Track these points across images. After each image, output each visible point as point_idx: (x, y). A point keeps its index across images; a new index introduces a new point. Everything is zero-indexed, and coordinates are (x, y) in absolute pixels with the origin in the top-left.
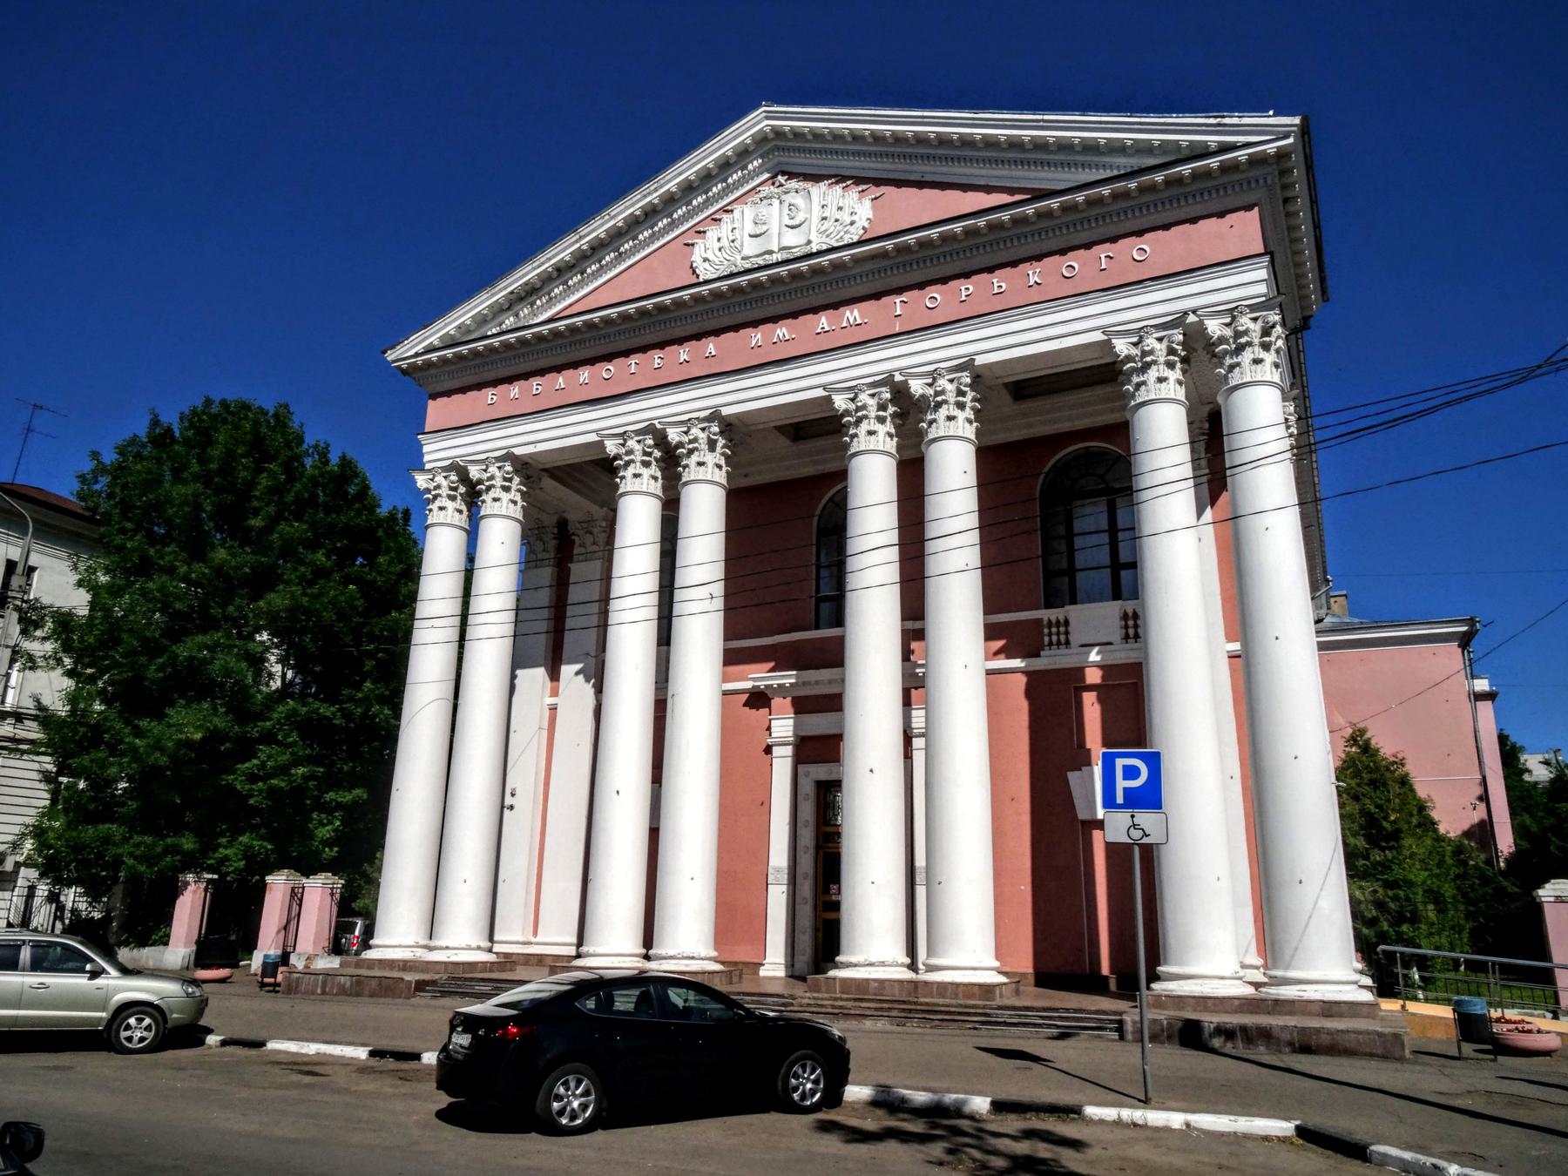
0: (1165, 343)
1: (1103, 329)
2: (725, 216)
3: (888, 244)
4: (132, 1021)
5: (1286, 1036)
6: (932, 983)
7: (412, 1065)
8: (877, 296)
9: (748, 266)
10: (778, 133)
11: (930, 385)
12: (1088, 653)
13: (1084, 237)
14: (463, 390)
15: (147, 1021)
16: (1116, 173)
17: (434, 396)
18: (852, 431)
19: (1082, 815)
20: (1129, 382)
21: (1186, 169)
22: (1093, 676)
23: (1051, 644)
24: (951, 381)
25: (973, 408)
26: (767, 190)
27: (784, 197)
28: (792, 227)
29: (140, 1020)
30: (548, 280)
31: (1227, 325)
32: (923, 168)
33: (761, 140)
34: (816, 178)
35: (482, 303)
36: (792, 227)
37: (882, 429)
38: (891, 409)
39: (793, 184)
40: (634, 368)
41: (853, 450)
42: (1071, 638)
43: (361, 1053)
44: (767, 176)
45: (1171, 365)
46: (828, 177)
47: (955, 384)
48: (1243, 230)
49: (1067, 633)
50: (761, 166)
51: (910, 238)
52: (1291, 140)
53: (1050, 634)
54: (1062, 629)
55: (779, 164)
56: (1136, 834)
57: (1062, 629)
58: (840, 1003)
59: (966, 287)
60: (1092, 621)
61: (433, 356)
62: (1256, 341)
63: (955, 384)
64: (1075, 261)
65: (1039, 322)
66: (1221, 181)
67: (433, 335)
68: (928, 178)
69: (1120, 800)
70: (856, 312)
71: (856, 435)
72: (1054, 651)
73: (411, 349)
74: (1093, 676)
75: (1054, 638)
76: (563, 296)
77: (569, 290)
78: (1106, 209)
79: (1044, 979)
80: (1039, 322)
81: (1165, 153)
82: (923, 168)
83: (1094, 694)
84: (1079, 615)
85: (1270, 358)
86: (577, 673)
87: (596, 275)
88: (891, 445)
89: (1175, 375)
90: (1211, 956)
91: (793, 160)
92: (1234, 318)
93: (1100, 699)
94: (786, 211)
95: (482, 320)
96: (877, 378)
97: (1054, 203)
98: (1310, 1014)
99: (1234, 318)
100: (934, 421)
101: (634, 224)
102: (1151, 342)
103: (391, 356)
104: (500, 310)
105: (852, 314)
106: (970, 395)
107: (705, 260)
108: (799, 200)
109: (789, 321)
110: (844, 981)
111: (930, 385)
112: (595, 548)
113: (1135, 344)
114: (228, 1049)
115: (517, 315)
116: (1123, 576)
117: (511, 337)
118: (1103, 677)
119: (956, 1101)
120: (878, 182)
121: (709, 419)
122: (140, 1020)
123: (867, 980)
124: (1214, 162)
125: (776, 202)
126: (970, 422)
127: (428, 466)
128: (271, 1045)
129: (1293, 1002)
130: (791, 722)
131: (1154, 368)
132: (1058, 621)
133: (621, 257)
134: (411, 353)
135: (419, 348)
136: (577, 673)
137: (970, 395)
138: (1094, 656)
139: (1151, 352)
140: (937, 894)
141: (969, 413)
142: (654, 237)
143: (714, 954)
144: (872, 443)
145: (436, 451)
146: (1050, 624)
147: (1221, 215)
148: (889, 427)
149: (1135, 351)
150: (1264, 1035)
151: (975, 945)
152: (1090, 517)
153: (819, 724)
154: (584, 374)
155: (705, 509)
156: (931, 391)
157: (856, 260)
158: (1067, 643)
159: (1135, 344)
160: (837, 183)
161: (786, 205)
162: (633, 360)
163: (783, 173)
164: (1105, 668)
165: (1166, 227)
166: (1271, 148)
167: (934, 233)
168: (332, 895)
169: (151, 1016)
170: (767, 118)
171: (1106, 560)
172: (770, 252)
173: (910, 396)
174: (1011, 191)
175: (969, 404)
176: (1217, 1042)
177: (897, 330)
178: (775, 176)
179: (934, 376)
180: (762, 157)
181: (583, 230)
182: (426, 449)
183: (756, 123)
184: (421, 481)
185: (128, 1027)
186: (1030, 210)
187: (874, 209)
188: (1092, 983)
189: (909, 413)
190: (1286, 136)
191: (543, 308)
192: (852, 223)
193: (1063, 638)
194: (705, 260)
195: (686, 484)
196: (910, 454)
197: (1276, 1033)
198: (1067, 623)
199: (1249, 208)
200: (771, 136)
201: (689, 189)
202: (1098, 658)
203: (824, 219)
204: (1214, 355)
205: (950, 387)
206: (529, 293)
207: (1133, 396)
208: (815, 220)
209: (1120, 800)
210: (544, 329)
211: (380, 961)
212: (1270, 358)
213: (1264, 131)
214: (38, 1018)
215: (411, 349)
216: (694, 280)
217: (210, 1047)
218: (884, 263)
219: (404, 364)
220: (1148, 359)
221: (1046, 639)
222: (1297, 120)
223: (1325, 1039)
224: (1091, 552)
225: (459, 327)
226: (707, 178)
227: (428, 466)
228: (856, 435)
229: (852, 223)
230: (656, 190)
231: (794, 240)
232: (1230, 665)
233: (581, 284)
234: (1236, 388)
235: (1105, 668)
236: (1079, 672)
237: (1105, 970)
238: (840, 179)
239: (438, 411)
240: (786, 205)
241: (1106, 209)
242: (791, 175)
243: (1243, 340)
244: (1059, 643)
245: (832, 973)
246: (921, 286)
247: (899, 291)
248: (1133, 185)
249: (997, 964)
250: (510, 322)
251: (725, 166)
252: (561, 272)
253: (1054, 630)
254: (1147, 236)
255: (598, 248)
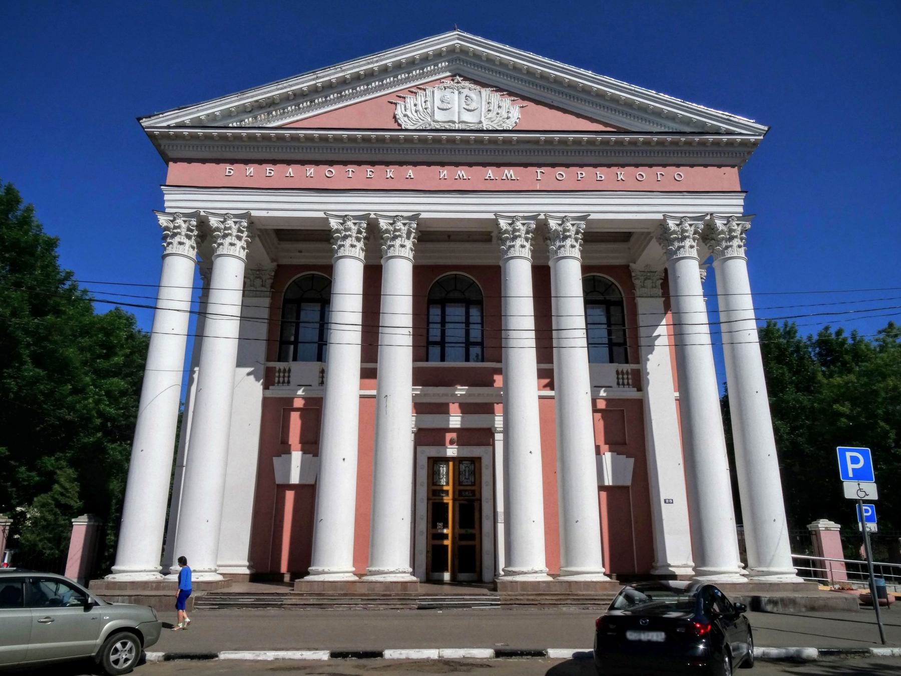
0: (237, 226)
1: (325, 211)
2: (421, 92)
3: (543, 136)
4: (118, 645)
5: (803, 602)
6: (580, 582)
7: (376, 662)
8: (526, 165)
9: (438, 127)
10: (464, 51)
11: (222, 222)
12: (297, 390)
13: (622, 160)
14: (204, 161)
15: (118, 645)
16: (667, 130)
17: (176, 161)
18: (219, 241)
19: (279, 480)
20: (504, 244)
21: (711, 138)
22: (299, 403)
23: (279, 382)
24: (355, 224)
25: (246, 241)
26: (448, 82)
27: (461, 90)
28: (468, 110)
29: (124, 644)
30: (287, 99)
31: (725, 225)
32: (554, 97)
33: (452, 50)
34: (484, 85)
35: (232, 102)
36: (468, 110)
37: (188, 243)
38: (196, 233)
39: (467, 84)
40: (336, 174)
41: (218, 253)
42: (291, 379)
43: (485, 653)
44: (448, 74)
45: (358, 239)
46: (492, 86)
47: (187, 224)
48: (730, 177)
49: (289, 377)
50: (446, 67)
51: (557, 136)
52: (762, 137)
53: (279, 377)
54: (287, 374)
55: (458, 69)
56: (862, 494)
57: (287, 374)
58: (530, 597)
59: (601, 172)
60: (302, 370)
61: (186, 131)
62: (523, 235)
63: (187, 224)
64: (643, 172)
65: (625, 201)
66: (501, 147)
67: (187, 115)
68: (555, 104)
69: (851, 475)
70: (511, 172)
71: (222, 244)
72: (281, 387)
73: (164, 121)
74: (299, 403)
75: (281, 380)
76: (293, 114)
77: (299, 110)
78: (414, 146)
79: (255, 578)
80: (625, 201)
81: (696, 127)
82: (554, 97)
83: (299, 413)
84: (297, 368)
85: (239, 244)
86: (249, 374)
87: (320, 105)
88: (193, 254)
89: (360, 245)
90: (335, 560)
91: (468, 69)
92: (728, 222)
93: (301, 417)
94: (463, 99)
95: (228, 114)
96: (526, 214)
97: (627, 138)
98: (787, 591)
99: (728, 222)
100: (171, 243)
101: (357, 79)
102: (519, 225)
103: (145, 122)
104: (244, 111)
105: (509, 172)
106: (245, 234)
107: (405, 115)
108: (473, 95)
109: (467, 168)
110: (524, 583)
111: (222, 222)
112: (263, 289)
113: (510, 224)
114: (172, 663)
115: (256, 118)
116: (320, 350)
117: (244, 132)
118: (305, 405)
119: (797, 651)
120: (524, 98)
121: (411, 218)
122: (124, 644)
123: (539, 582)
124: (725, 138)
125: (456, 92)
126: (244, 248)
127: (167, 210)
128: (223, 656)
129: (778, 584)
130: (459, 419)
131: (350, 239)
132: (285, 370)
133: (341, 98)
134: (165, 124)
135: (172, 123)
136: (249, 374)
137: (196, 233)
138: (300, 392)
139: (399, 230)
140: (367, 529)
141: (243, 243)
142: (366, 92)
143: (354, 569)
144: (181, 250)
145: (174, 200)
146: (279, 371)
147: (719, 166)
148: (192, 242)
149: (510, 228)
150: (793, 602)
151: (218, 549)
152: (310, 313)
153: (432, 421)
154: (311, 170)
155: (231, 272)
156: (222, 226)
157: (519, 141)
158: (289, 382)
159: (560, 225)
160: (496, 91)
161: (463, 96)
162: (351, 168)
163: (460, 76)
164: (607, 400)
165: (692, 166)
166: (752, 138)
167: (557, 136)
168: (4, 531)
169: (134, 641)
170: (458, 39)
171: (463, 340)
172: (454, 122)
173: (209, 227)
174: (606, 124)
175: (244, 238)
176: (769, 608)
177: (538, 188)
178: (455, 76)
179: (564, 220)
180: (449, 62)
181: (320, 73)
182: (166, 197)
183: (450, 39)
184: (163, 220)
185: (116, 651)
186: (613, 138)
187: (522, 113)
188: (277, 579)
189: (375, 240)
190: (760, 135)
191: (277, 118)
192: (508, 118)
193: (286, 379)
194: (405, 115)
195: (220, 256)
196: (373, 262)
197: (797, 600)
198: (289, 371)
199: (733, 166)
200: (458, 50)
201: (399, 67)
202: (605, 395)
203: (489, 110)
204: (501, 239)
205: (184, 226)
206: (270, 105)
207: (337, 252)
208: (484, 111)
209: (851, 475)
210: (273, 133)
211: (133, 583)
212: (239, 244)
213: (746, 127)
214: (43, 650)
215: (164, 121)
216: (397, 127)
217: (153, 662)
218: (535, 147)
219: (156, 132)
220: (397, 233)
221: (277, 379)
222: (766, 128)
223: (822, 603)
224: (308, 333)
225: (208, 115)
226: (412, 63)
227: (167, 210)
228: (222, 244)
229: (508, 118)
230: (377, 62)
231: (470, 119)
232: (360, 403)
233: (309, 109)
234: (512, 258)
235: (607, 400)
236: (290, 401)
237: (284, 568)
238: (499, 89)
239: (176, 172)
240: (463, 96)
241: (414, 146)
242: (466, 79)
243: (397, 233)
244: (284, 382)
245: (308, 578)
246: (553, 165)
247: (540, 165)
248: (683, 139)
249: (354, 569)
250: (248, 121)
251: (426, 59)
252: (298, 97)
253: (625, 376)
254: (681, 168)
255: (329, 87)
